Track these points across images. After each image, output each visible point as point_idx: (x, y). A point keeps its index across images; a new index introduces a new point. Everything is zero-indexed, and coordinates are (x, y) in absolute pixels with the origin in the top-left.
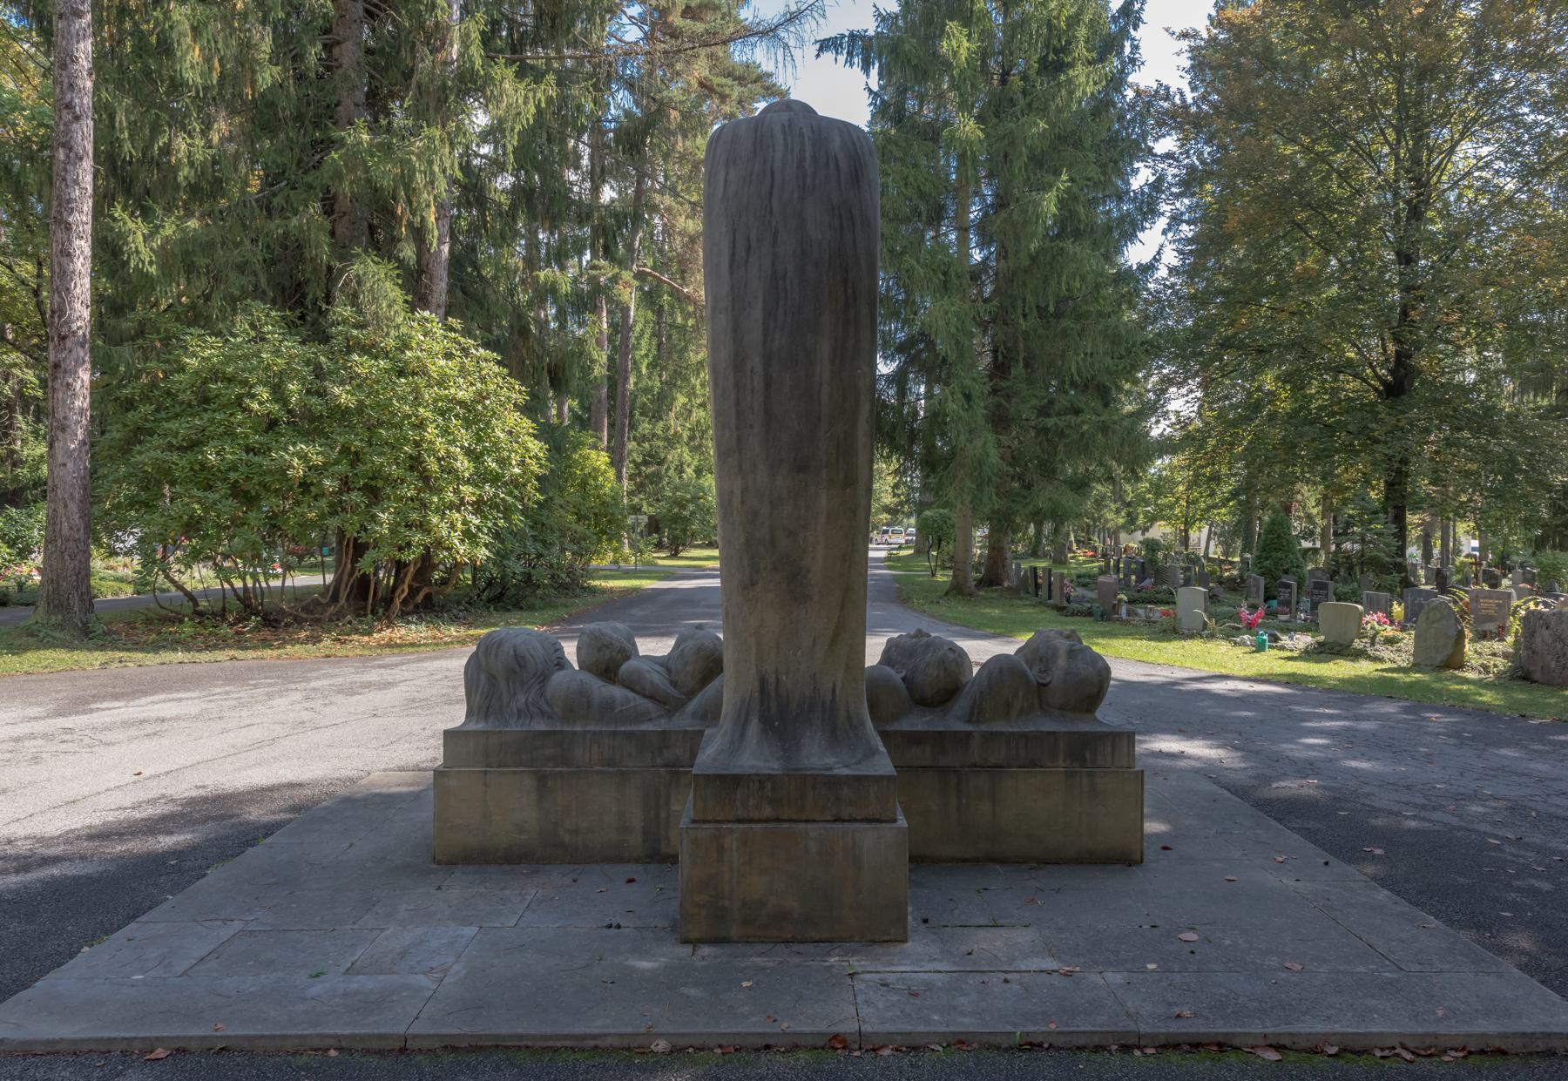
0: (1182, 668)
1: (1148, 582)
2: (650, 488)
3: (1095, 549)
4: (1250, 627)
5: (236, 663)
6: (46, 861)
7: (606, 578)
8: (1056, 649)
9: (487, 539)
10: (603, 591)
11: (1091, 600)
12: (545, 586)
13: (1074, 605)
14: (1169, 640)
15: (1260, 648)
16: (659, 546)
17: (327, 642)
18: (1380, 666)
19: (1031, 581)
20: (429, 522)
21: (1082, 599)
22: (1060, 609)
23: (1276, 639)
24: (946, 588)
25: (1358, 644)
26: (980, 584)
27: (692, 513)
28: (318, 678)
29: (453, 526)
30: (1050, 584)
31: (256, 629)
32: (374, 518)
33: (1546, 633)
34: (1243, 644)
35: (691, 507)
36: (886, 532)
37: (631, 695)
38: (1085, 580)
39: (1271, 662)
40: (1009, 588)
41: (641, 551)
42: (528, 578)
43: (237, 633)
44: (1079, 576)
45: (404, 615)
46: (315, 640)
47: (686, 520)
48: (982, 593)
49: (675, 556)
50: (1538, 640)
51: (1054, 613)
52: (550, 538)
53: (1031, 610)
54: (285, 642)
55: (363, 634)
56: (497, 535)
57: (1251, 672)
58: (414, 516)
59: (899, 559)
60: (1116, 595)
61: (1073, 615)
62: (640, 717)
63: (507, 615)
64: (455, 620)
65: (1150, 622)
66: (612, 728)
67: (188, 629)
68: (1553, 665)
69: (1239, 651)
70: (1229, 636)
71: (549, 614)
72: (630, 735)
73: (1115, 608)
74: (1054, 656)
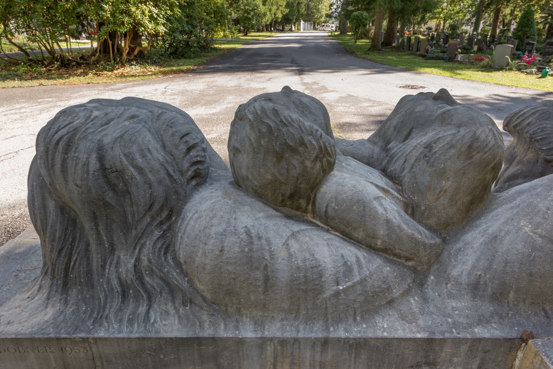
2: (235, 5)
5: (42, 87)
6: (175, 72)
7: (221, 44)
9: (163, 21)
10: (220, 50)
12: (195, 47)
13: (429, 55)
16: (240, 31)
17: (91, 75)
20: (130, 10)
21: (433, 52)
22: (423, 56)
24: (369, 46)
27: (253, 16)
28: (76, 98)
29: (143, 13)
31: (58, 69)
32: (102, 8)
34: (531, 73)
36: (323, 26)
37: (351, 252)
40: (394, 47)
42: (187, 44)
43: (50, 70)
45: (129, 61)
46: (85, 74)
47: (250, 19)
49: (246, 35)
51: (421, 58)
52: (195, 23)
53: (409, 57)
54: (70, 75)
55: (109, 71)
56: (168, 19)
58: (123, 7)
59: (335, 36)
61: (430, 59)
62: (374, 301)
63: (178, 61)
64: (154, 63)
66: (317, 332)
67: (22, 69)
71: (198, 60)
72: (357, 345)
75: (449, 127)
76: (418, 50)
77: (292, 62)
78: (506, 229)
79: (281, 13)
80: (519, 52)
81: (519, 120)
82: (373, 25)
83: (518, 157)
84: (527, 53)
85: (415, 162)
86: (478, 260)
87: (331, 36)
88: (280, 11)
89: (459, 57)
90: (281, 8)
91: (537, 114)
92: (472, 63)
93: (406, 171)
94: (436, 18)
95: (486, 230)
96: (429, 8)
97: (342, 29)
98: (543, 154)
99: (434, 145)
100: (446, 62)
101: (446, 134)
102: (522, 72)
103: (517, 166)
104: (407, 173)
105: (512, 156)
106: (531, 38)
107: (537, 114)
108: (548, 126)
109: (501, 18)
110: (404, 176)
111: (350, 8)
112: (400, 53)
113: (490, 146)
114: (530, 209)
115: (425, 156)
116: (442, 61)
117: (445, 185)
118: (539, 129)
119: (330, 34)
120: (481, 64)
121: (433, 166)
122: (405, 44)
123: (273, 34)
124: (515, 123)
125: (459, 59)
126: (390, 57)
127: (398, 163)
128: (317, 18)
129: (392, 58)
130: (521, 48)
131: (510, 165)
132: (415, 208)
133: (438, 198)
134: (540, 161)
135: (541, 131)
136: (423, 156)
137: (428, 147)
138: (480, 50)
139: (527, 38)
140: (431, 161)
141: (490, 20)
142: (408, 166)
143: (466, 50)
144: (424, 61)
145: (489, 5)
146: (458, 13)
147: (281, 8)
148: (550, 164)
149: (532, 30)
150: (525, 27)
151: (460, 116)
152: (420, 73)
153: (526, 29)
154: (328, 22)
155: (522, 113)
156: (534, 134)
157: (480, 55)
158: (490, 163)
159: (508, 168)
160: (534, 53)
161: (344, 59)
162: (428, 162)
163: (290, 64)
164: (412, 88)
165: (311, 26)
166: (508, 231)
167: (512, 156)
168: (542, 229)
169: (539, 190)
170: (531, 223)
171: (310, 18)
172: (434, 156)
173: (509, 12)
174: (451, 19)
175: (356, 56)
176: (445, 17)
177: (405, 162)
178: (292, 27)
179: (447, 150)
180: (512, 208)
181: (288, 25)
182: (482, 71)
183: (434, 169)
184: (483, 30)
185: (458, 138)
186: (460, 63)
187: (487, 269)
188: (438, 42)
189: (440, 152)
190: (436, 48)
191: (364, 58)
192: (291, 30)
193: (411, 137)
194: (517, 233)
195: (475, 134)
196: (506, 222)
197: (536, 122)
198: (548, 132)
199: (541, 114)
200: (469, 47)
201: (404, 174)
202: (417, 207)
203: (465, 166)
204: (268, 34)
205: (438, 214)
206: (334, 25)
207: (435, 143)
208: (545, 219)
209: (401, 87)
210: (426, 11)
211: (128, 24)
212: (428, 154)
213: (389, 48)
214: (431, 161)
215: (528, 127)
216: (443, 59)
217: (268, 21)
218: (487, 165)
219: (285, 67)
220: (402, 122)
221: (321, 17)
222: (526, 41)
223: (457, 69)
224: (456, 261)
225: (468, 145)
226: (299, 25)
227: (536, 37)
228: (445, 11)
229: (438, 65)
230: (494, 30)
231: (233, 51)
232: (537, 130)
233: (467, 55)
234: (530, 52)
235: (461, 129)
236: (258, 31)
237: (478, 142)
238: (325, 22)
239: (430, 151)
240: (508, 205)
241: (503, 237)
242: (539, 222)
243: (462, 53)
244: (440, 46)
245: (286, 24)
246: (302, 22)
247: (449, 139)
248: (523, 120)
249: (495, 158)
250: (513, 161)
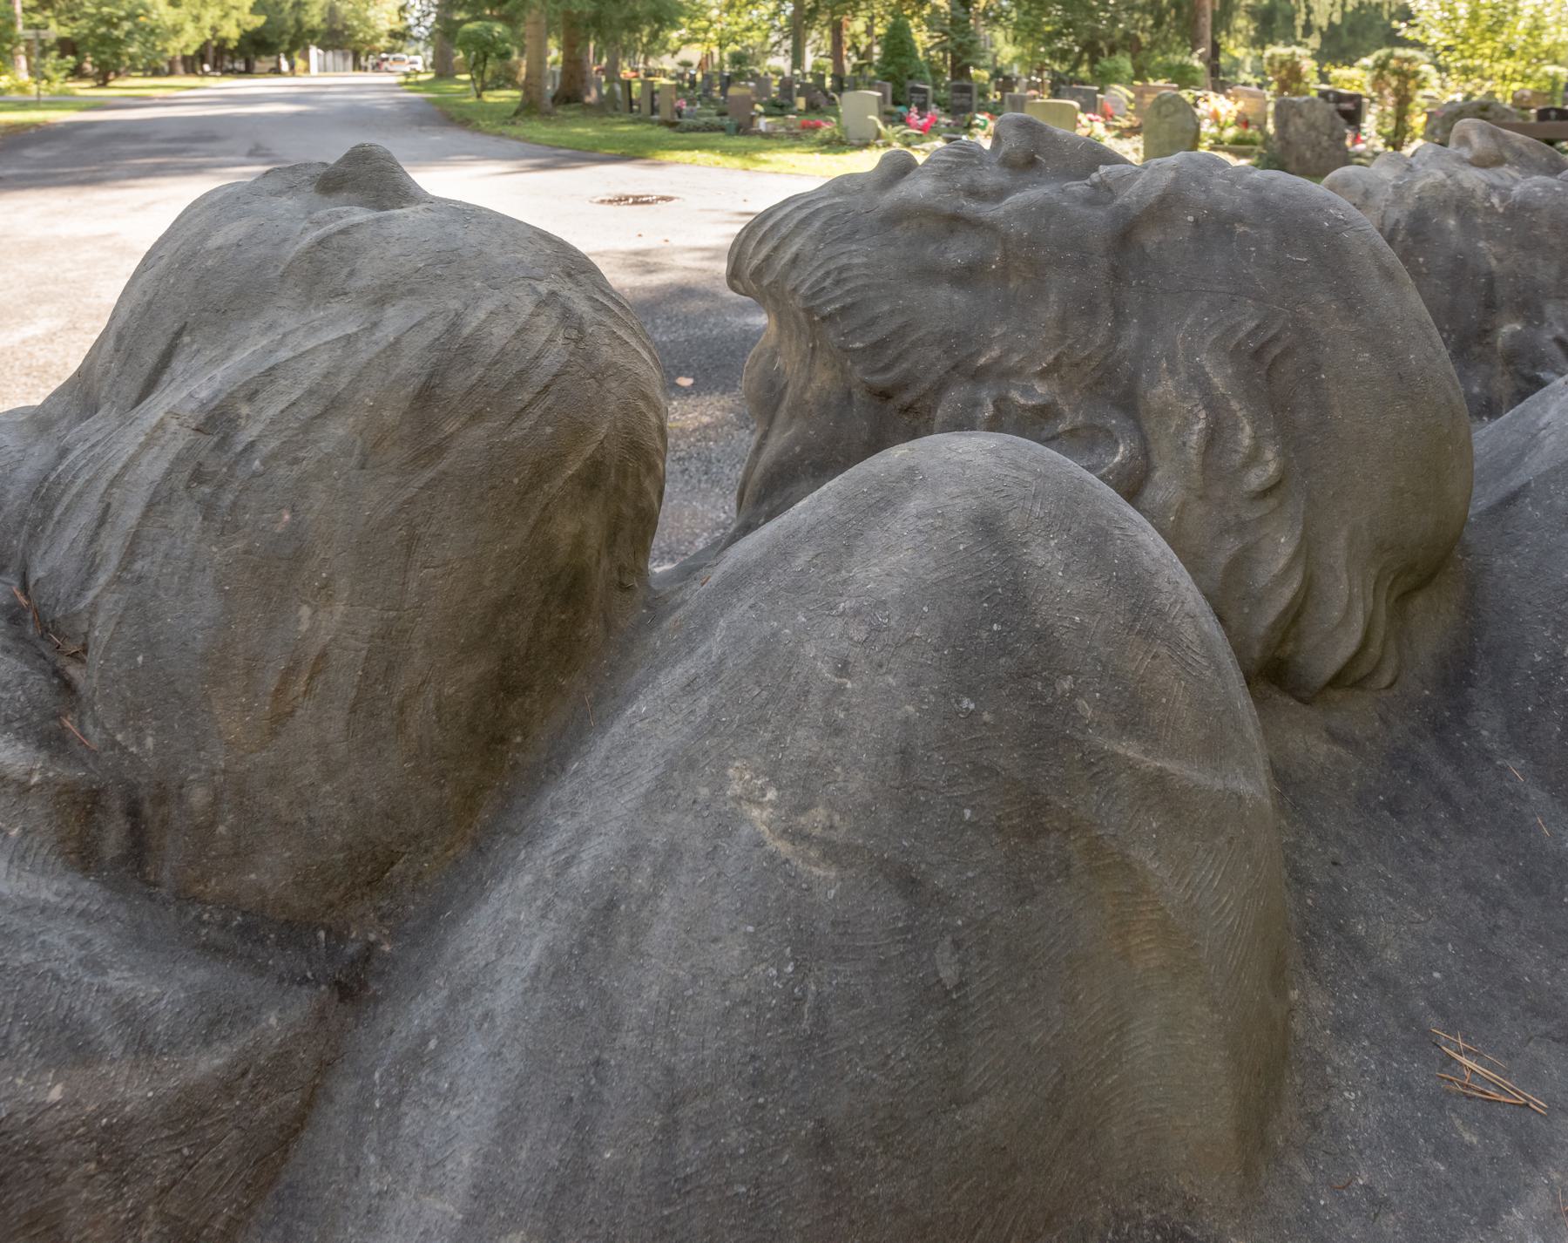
13: (686, 121)
16: (77, 73)
22: (671, 125)
24: (515, 107)
27: (129, 34)
33: (1299, 121)
35: (127, 25)
48: (559, 111)
50: (1292, 129)
61: (689, 130)
68: (1308, 155)
75: (336, 307)
76: (654, 110)
77: (251, 154)
78: (658, 840)
79: (238, 26)
80: (901, 109)
81: (765, 250)
82: (522, 54)
83: (790, 389)
84: (914, 109)
85: (145, 515)
86: (509, 1128)
87: (406, 83)
88: (233, 22)
89: (763, 123)
90: (234, 13)
91: (817, 224)
92: (797, 137)
93: (102, 578)
94: (697, 41)
95: (568, 863)
96: (664, 18)
97: (443, 68)
98: (858, 368)
99: (245, 410)
101: (309, 345)
103: (789, 425)
104: (109, 584)
105: (772, 386)
107: (817, 224)
108: (856, 261)
109: (848, 42)
110: (94, 608)
111: (459, 16)
112: (607, 119)
113: (539, 378)
114: (766, 680)
115: (198, 476)
116: (721, 134)
117: (314, 630)
118: (828, 274)
119: (402, 79)
120: (818, 136)
121: (237, 528)
122: (620, 98)
123: (209, 81)
124: (755, 262)
125: (762, 127)
126: (579, 130)
127: (71, 533)
128: (364, 41)
129: (585, 131)
131: (771, 422)
132: (147, 809)
133: (280, 719)
134: (858, 395)
135: (837, 283)
136: (186, 475)
137: (217, 421)
138: (812, 107)
139: (910, 77)
140: (228, 498)
141: (827, 45)
142: (112, 545)
143: (778, 108)
144: (673, 135)
145: (814, 12)
146: (748, 29)
147: (234, 13)
148: (891, 405)
150: (901, 55)
151: (396, 250)
152: (661, 164)
153: (903, 60)
154: (400, 51)
155: (770, 223)
156: (814, 296)
157: (813, 118)
158: (559, 459)
159: (765, 436)
160: (934, 110)
161: (438, 138)
162: (208, 509)
163: (243, 159)
164: (635, 203)
166: (674, 850)
167: (772, 386)
168: (831, 804)
169: (800, 562)
170: (774, 780)
171: (341, 39)
172: (241, 473)
173: (863, 28)
174: (737, 42)
175: (478, 130)
176: (720, 39)
177: (102, 522)
178: (278, 63)
179: (307, 427)
180: (690, 687)
181: (264, 58)
182: (823, 152)
183: (239, 545)
184: (816, 66)
185: (363, 357)
186: (767, 136)
187: (561, 1189)
188: (707, 91)
189: (274, 444)
190: (706, 105)
191: (501, 135)
192: (277, 71)
193: (166, 378)
194: (712, 855)
195: (454, 326)
196: (662, 784)
197: (817, 250)
198: (860, 282)
199: (827, 224)
200: (786, 102)
201: (90, 595)
202: (161, 799)
203: (411, 501)
205: (301, 815)
206: (419, 59)
207: (251, 397)
208: (838, 731)
209: (603, 201)
210: (659, 20)
212: (210, 466)
214: (228, 498)
215: (794, 274)
216: (722, 129)
217: (187, 46)
218: (541, 472)
219: (220, 166)
220: (150, 303)
221: (377, 38)
222: (909, 84)
223: (760, 149)
224: (387, 1162)
225: (414, 385)
226: (306, 57)
227: (928, 76)
228: (718, 26)
230: (838, 64)
231: (32, 131)
232: (824, 278)
233: (780, 120)
234: (923, 108)
235: (390, 311)
236: (157, 72)
237: (471, 363)
238: (390, 51)
239: (223, 444)
240: (679, 670)
241: (645, 899)
242: (811, 763)
243: (767, 114)
244: (714, 101)
245: (257, 55)
246: (314, 52)
247: (322, 363)
248: (776, 249)
249: (580, 431)
250: (776, 408)
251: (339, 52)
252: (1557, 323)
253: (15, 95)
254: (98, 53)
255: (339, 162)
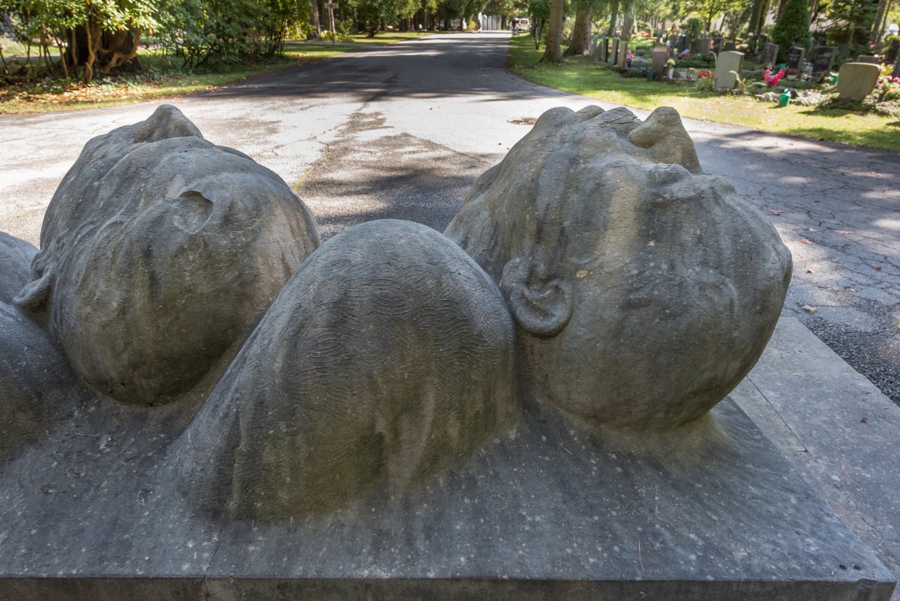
0: (724, 124)
1: (686, 51)
3: (649, 31)
4: (771, 85)
8: (599, 191)
11: (647, 65)
13: (633, 69)
14: (706, 97)
15: (782, 103)
18: (886, 120)
19: (603, 51)
21: (639, 65)
23: (794, 95)
25: (869, 100)
26: (566, 53)
30: (617, 53)
34: (767, 100)
38: (642, 51)
39: (792, 117)
40: (587, 57)
41: (341, 32)
44: (638, 48)
45: (99, 79)
49: (371, 36)
51: (618, 75)
53: (600, 73)
57: (783, 128)
60: (667, 59)
61: (632, 76)
65: (690, 82)
69: (765, 106)
70: (754, 93)
73: (665, 70)
74: (591, 223)
100: (649, 81)
102: (756, 98)
106: (802, 42)
123: (422, 36)
130: (785, 58)
149: (803, 28)
150: (793, 23)
153: (794, 27)
165: (498, 22)
176: (711, 8)
178: (461, 24)
192: (460, 29)
204: (414, 35)
211: (80, 13)
213: (577, 58)
217: (410, 13)
229: (626, 86)
251: (495, 16)
252: (22, 2)
253: (329, 42)
254: (367, 21)
255: (579, 112)
